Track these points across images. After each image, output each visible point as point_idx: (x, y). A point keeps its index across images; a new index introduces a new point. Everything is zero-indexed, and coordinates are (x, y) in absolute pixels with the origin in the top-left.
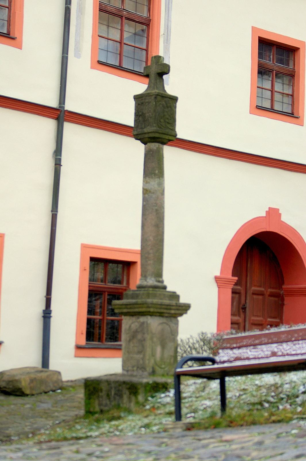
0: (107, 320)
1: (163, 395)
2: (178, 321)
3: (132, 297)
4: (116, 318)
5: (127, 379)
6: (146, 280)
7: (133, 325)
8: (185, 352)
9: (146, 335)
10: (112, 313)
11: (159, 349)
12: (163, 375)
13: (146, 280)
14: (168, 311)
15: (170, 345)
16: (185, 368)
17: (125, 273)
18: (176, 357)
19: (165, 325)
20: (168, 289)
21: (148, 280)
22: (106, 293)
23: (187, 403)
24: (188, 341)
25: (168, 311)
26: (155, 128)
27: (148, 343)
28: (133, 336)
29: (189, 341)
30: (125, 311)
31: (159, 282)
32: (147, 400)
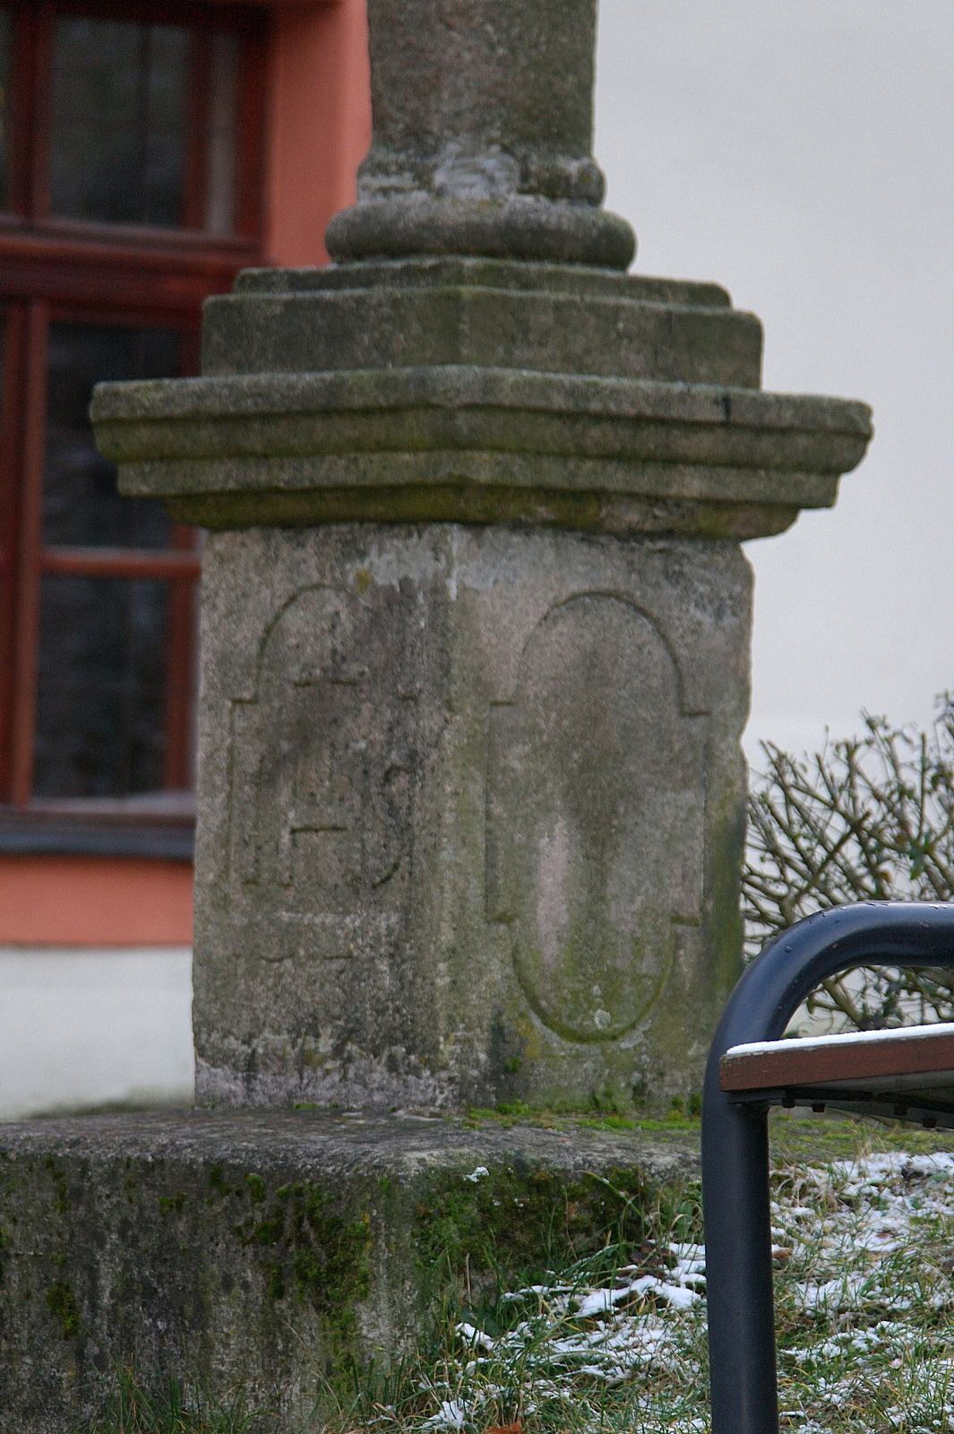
0: (51, 573)
1: (597, 1300)
2: (746, 577)
3: (291, 352)
4: (136, 558)
5: (240, 1143)
6: (423, 179)
7: (295, 620)
8: (814, 874)
9: (429, 720)
10: (105, 507)
11: (556, 855)
12: (598, 1106)
13: (423, 179)
14: (645, 481)
15: (674, 812)
16: (815, 1030)
17: (222, 114)
18: (722, 927)
19: (614, 613)
20: (643, 266)
21: (439, 178)
22: (39, 316)
23: (834, 1369)
24: (840, 772)
25: (645, 481)
26: (238, 1089)
27: (451, 795)
28: (302, 732)
29: (853, 770)
30: (220, 476)
31: (554, 187)
32: (441, 1344)
